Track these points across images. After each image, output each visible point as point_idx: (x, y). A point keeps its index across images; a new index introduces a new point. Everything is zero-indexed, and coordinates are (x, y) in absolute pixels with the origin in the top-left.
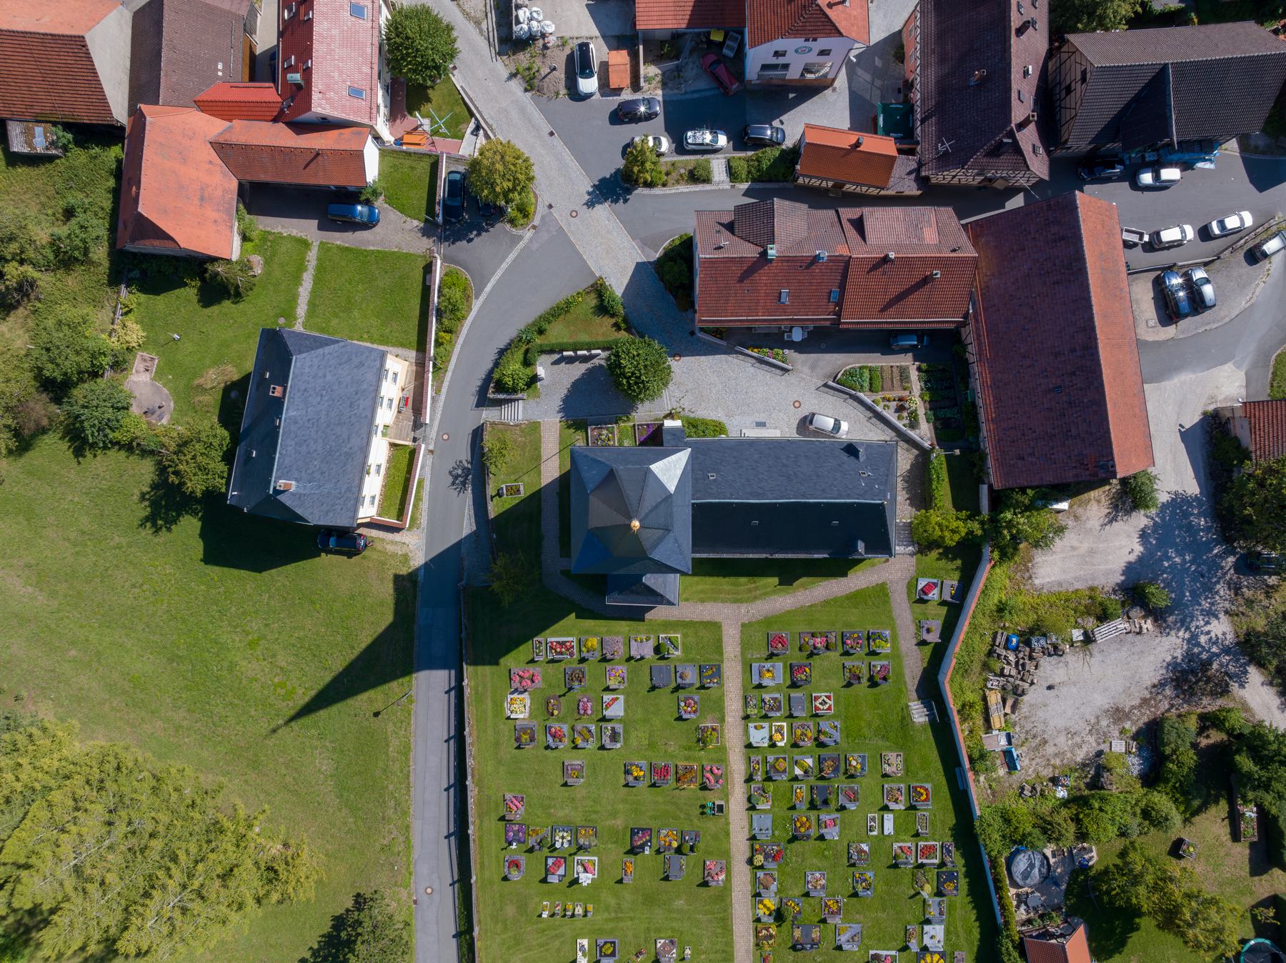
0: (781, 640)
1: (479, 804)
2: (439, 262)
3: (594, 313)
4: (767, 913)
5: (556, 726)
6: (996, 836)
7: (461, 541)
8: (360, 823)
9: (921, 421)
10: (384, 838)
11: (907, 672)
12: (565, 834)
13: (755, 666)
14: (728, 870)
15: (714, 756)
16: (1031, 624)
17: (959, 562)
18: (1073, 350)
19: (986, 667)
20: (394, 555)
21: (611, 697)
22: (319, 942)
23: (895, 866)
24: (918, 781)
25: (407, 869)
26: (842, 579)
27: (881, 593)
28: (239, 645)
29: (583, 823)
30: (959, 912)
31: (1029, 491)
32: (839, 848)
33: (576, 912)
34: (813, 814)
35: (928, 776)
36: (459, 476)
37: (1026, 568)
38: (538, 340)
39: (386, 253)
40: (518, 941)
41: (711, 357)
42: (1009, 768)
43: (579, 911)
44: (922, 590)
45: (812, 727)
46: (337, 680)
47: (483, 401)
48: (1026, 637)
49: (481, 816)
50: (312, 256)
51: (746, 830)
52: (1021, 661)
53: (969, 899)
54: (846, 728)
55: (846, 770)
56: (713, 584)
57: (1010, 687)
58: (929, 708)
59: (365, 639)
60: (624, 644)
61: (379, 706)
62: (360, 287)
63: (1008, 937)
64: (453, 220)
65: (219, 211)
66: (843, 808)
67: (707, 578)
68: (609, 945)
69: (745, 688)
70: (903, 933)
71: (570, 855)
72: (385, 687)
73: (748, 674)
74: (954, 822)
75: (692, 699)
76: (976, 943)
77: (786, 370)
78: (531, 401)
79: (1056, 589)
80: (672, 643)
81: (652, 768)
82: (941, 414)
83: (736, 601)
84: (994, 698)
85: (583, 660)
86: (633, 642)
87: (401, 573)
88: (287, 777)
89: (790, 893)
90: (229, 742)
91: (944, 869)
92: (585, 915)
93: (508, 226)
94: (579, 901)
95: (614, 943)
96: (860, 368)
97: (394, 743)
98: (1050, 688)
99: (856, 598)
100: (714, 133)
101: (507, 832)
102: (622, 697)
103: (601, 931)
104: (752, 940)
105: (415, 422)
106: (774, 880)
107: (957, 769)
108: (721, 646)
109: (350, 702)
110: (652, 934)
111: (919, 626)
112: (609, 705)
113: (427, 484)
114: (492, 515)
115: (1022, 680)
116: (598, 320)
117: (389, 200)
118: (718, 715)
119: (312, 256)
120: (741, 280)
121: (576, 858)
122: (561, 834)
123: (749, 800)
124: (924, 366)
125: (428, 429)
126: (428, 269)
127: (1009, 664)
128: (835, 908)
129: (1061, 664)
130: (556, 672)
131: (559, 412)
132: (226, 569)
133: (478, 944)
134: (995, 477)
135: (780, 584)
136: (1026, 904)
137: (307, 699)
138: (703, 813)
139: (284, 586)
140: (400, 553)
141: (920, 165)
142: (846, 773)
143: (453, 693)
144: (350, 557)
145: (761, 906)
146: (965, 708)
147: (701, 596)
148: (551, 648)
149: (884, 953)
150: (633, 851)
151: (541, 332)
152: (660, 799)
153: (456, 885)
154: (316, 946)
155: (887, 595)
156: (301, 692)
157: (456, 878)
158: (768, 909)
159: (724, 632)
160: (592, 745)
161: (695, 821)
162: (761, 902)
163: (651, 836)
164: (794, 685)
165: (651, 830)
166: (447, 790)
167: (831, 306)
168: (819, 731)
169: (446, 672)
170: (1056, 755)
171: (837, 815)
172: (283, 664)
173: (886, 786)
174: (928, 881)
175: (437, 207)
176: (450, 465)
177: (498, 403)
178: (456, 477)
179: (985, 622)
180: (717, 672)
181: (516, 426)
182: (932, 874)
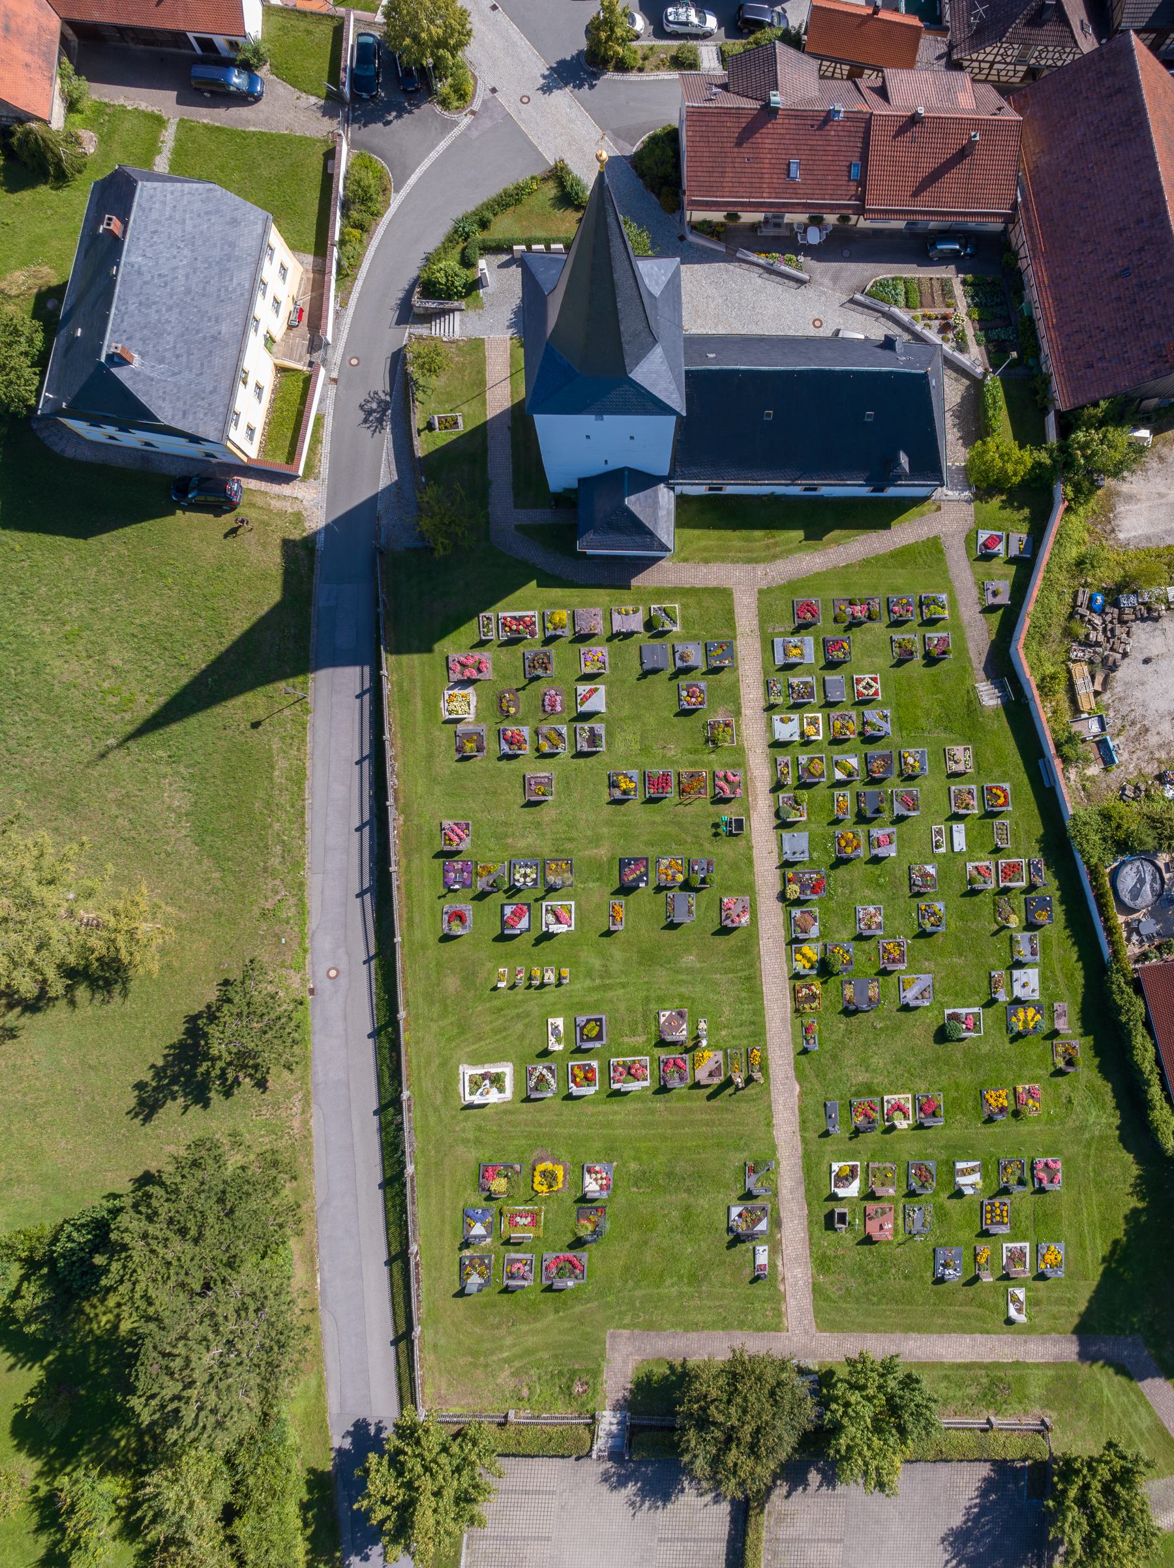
0: (809, 608)
1: (405, 838)
2: (345, 148)
3: (553, 206)
4: (808, 965)
5: (511, 729)
6: (1096, 838)
7: (377, 494)
8: (230, 878)
9: (970, 343)
10: (266, 898)
11: (971, 646)
12: (528, 871)
13: (778, 641)
14: (753, 910)
15: (729, 760)
16: (1118, 579)
17: (1026, 512)
18: (1140, 221)
19: (1068, 633)
20: (281, 514)
21: (588, 688)
22: (165, 1056)
23: (974, 893)
24: (993, 781)
25: (300, 944)
26: (882, 532)
27: (934, 548)
28: (51, 638)
29: (554, 855)
30: (1056, 952)
31: (1102, 403)
32: (898, 873)
33: (546, 981)
34: (861, 830)
35: (1005, 773)
36: (375, 411)
37: (1106, 514)
38: (479, 236)
39: (272, 135)
40: (463, 1028)
41: (707, 266)
42: (1105, 763)
43: (550, 977)
44: (984, 544)
45: (854, 718)
46: (199, 682)
47: (407, 314)
48: (1113, 595)
49: (407, 855)
50: (169, 136)
51: (775, 855)
52: (1110, 626)
53: (1068, 932)
54: (899, 718)
55: (901, 770)
56: (719, 539)
57: (1098, 660)
58: (1001, 687)
59: (240, 623)
60: (604, 619)
61: (260, 713)
62: (236, 176)
63: (1118, 971)
64: (365, 95)
65: (31, 52)
66: (900, 819)
67: (711, 532)
68: (593, 1024)
69: (766, 672)
70: (986, 983)
71: (536, 900)
72: (269, 689)
73: (769, 653)
74: (1042, 831)
75: (697, 686)
76: (1080, 990)
77: (801, 282)
78: (471, 313)
79: (1144, 544)
80: (667, 615)
81: (646, 778)
82: (994, 334)
83: (749, 561)
84: (1080, 671)
85: (548, 641)
86: (615, 616)
87: (291, 537)
88: (119, 820)
89: (837, 936)
90: (31, 775)
91: (1033, 895)
92: (559, 985)
93: (438, 109)
94: (549, 964)
95: (600, 1020)
96: (893, 279)
97: (281, 764)
98: (1147, 661)
99: (903, 556)
100: (700, 12)
101: (446, 871)
102: (602, 688)
103: (581, 1007)
104: (789, 1004)
105: (311, 341)
106: (815, 919)
107: (1040, 762)
108: (733, 618)
109: (217, 710)
110: (653, 1006)
111: (983, 589)
112: (585, 699)
113: (329, 422)
114: (420, 453)
115: (1112, 649)
116: (559, 213)
117: (276, 70)
118: (731, 707)
119: (169, 136)
120: (739, 144)
121: (544, 904)
122: (522, 871)
123: (777, 814)
124: (969, 277)
125: (330, 351)
126: (331, 155)
127: (1095, 629)
128: (896, 954)
129: (1157, 633)
130: (512, 658)
131: (509, 327)
132: (34, 536)
133: (404, 1036)
134: (1061, 398)
135: (806, 539)
136: (1139, 934)
137: (152, 709)
138: (716, 835)
139: (119, 556)
140: (290, 510)
141: (951, 47)
142: (901, 774)
143: (367, 697)
144: (217, 515)
145: (799, 957)
146: (1045, 687)
147: (705, 554)
148: (504, 625)
149: (963, 1011)
150: (625, 890)
151: (484, 225)
152: (658, 819)
153: (373, 963)
154: (160, 1063)
155: (941, 552)
156: (142, 700)
157: (372, 952)
158: (809, 960)
159: (736, 601)
160: (564, 751)
161: (707, 845)
162: (798, 951)
163: (646, 867)
164: (832, 665)
165: (647, 859)
166: (359, 829)
167: (853, 187)
168: (865, 723)
169: (358, 669)
170: (1160, 746)
171: (894, 829)
172: (118, 663)
173: (953, 788)
174: (1014, 912)
175: (342, 74)
176: (361, 396)
177: (427, 317)
178: (370, 413)
179: (1063, 577)
180: (728, 649)
181: (450, 342)
182: (1019, 901)
